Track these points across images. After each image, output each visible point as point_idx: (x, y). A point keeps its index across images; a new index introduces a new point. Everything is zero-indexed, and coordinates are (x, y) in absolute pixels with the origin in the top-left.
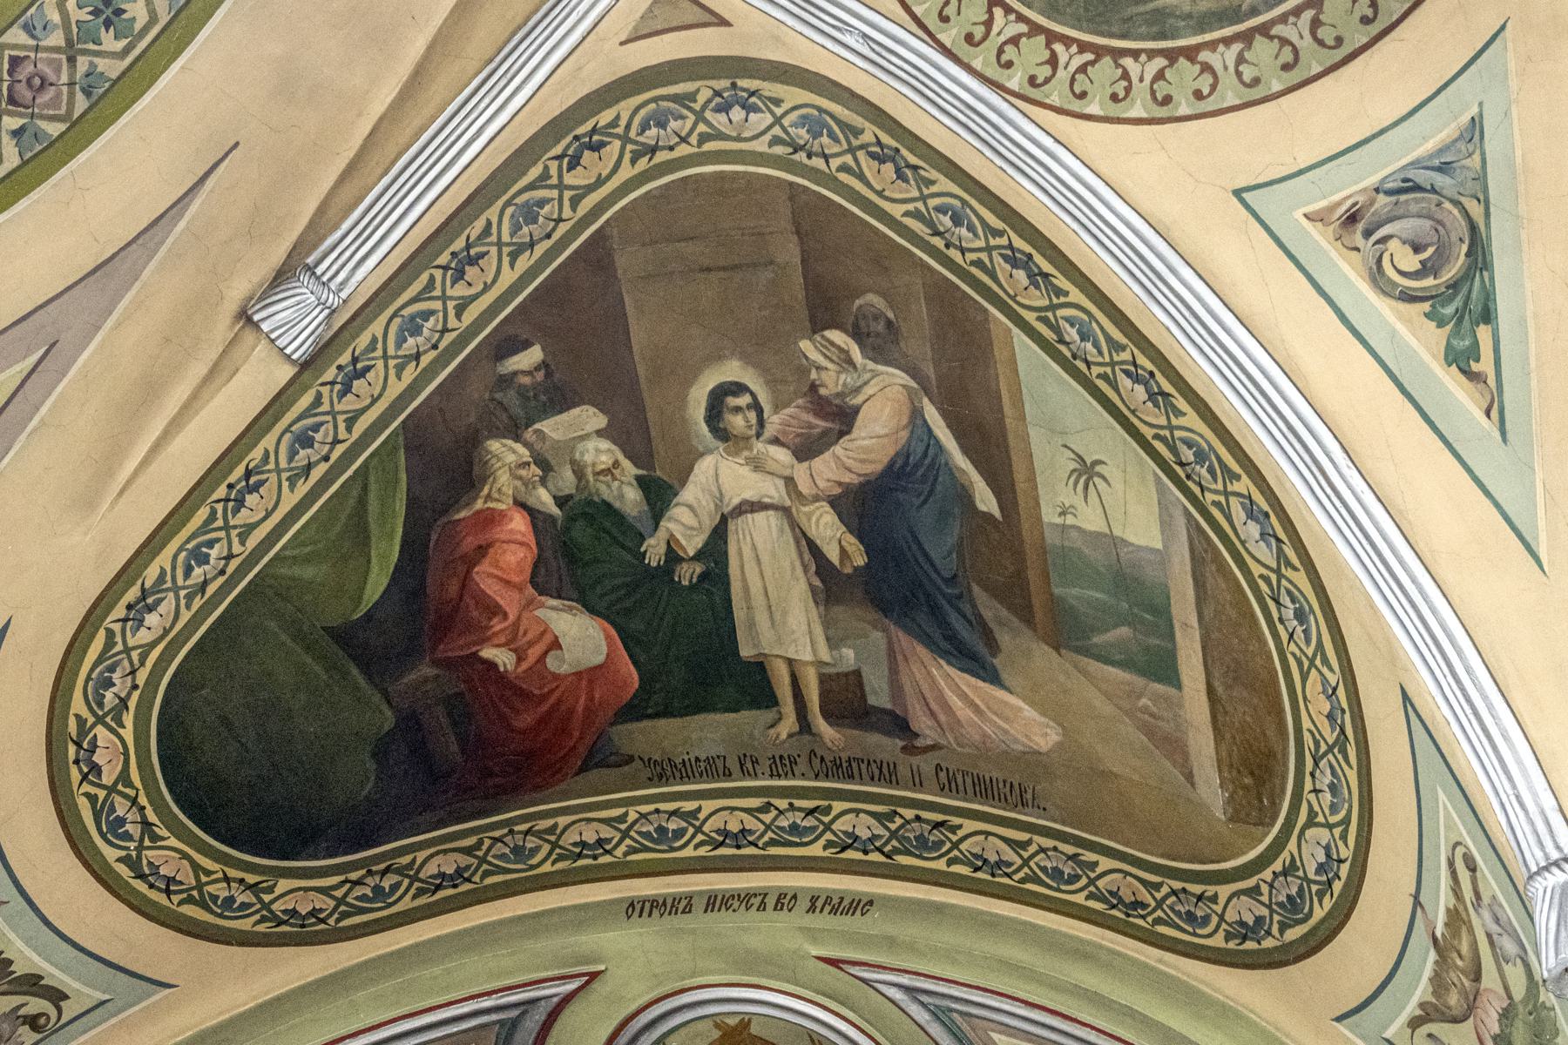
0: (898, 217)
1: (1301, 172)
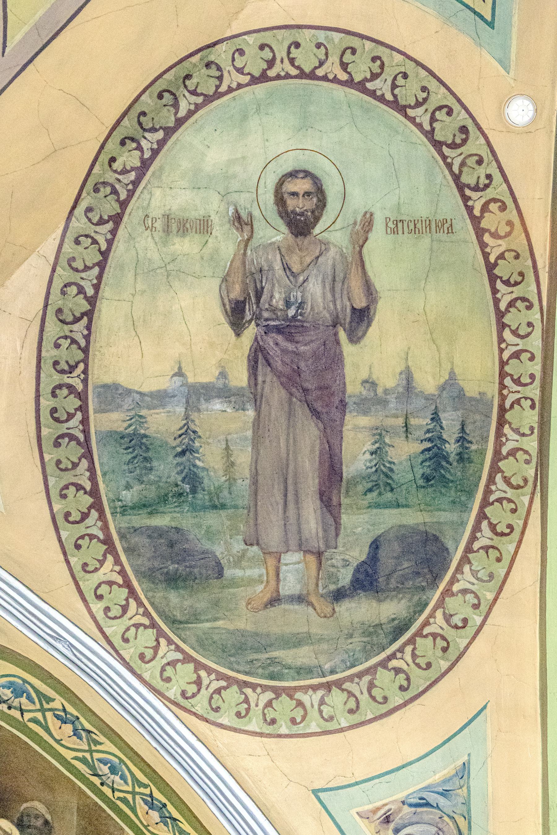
0: (69, 760)
1: (357, 783)
